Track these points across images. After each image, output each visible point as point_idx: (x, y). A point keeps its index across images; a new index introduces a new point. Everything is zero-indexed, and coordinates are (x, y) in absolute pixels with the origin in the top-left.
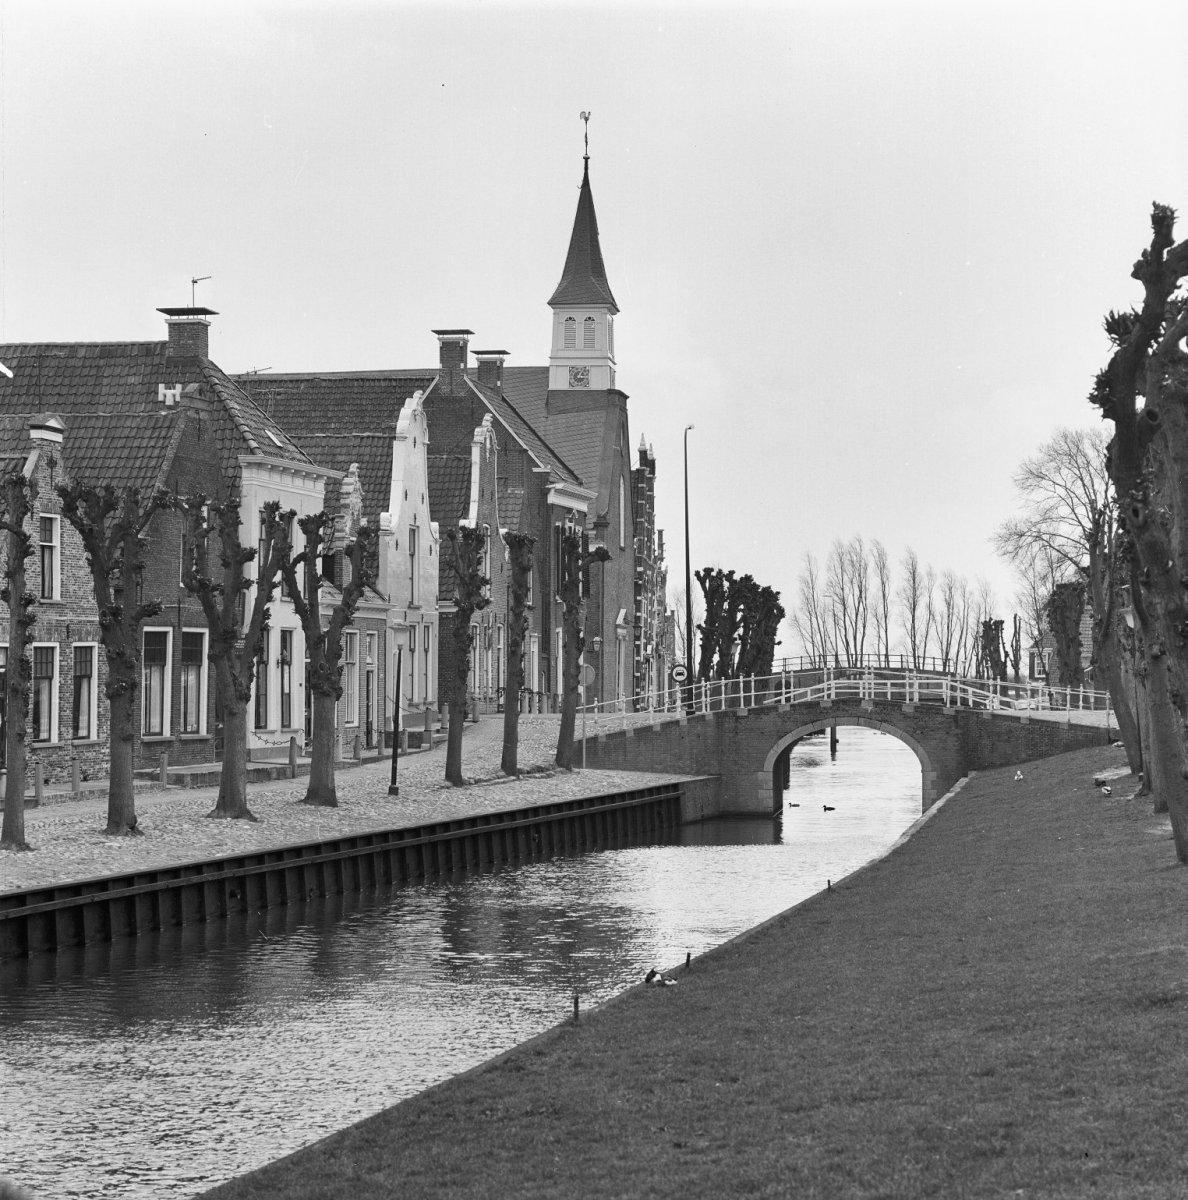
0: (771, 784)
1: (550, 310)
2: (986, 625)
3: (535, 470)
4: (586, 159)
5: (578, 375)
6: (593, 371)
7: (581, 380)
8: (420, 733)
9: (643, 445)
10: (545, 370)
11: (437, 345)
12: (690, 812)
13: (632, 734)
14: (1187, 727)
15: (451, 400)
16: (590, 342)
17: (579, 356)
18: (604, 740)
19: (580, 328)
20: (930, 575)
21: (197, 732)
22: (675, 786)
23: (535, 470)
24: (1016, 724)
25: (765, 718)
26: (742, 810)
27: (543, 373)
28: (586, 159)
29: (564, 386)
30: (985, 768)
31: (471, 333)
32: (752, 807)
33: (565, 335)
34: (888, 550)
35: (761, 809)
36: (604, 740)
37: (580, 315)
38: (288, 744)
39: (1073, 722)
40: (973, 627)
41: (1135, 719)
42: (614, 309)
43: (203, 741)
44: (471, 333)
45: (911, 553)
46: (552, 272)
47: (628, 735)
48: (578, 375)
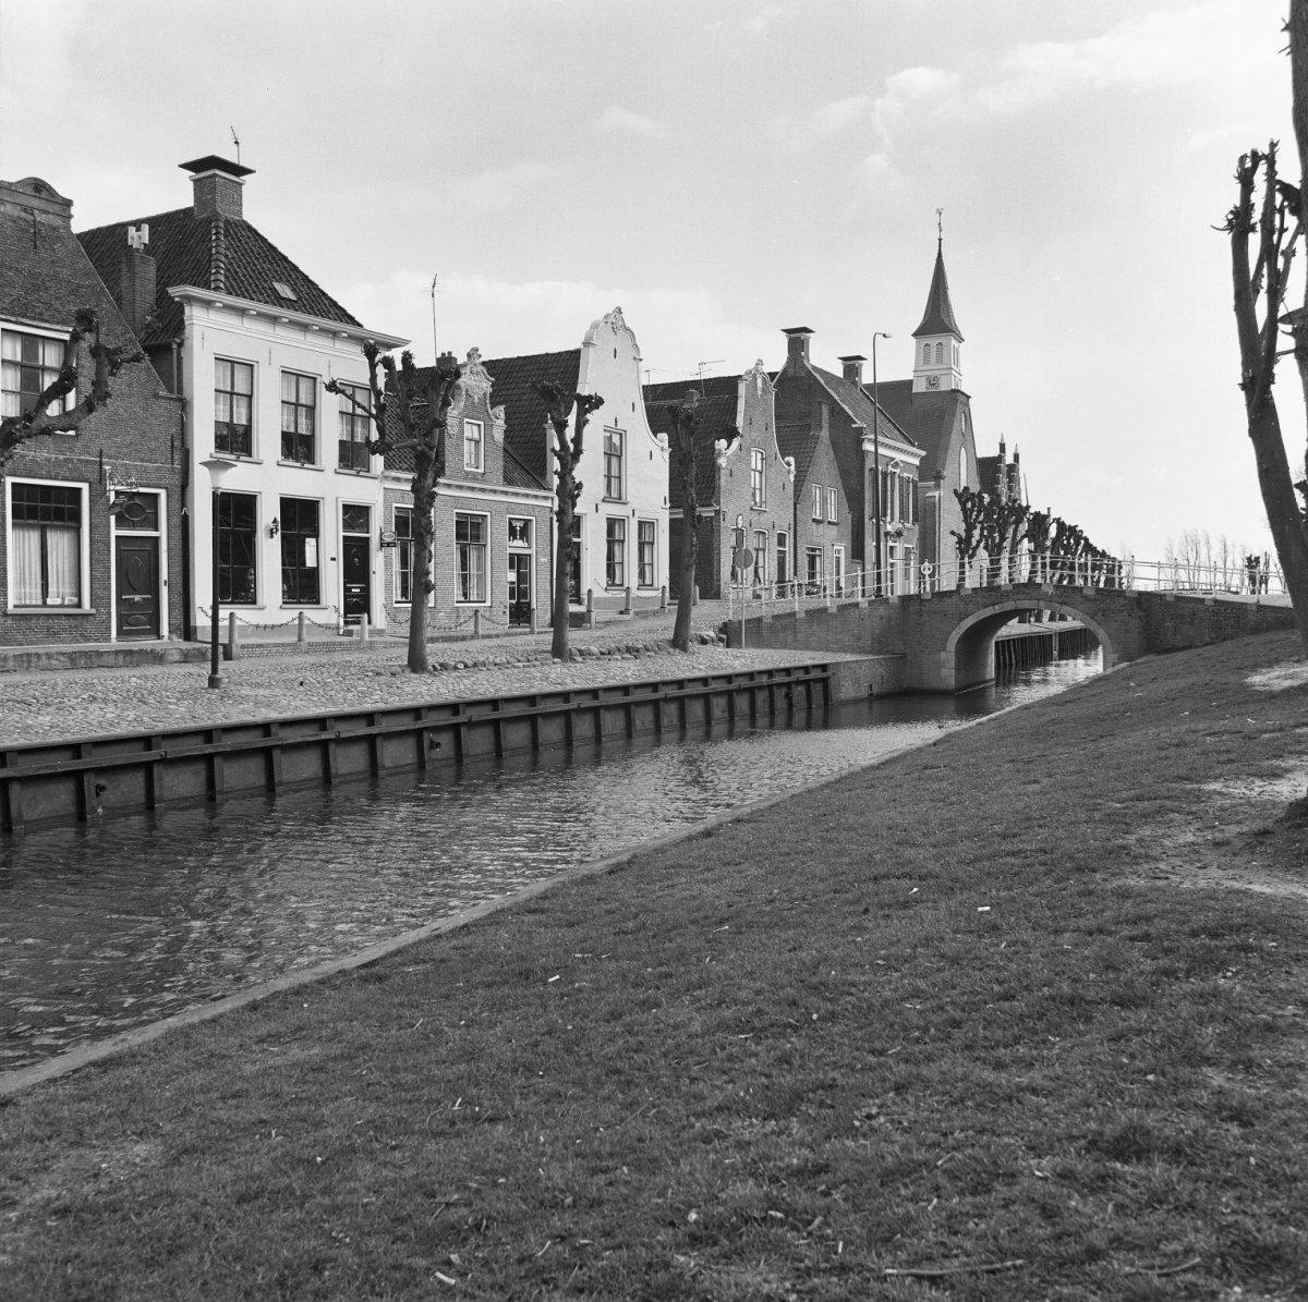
0: (953, 664)
1: (914, 340)
2: (1249, 559)
3: (854, 426)
4: (940, 240)
5: (932, 382)
6: (942, 378)
7: (934, 384)
8: (582, 614)
9: (1002, 439)
10: (911, 382)
11: (786, 341)
12: (846, 690)
13: (803, 615)
14: (110, 1289)
15: (795, 379)
16: (940, 359)
17: (933, 369)
18: (770, 620)
19: (933, 351)
20: (1233, 545)
21: (79, 605)
22: (824, 667)
23: (854, 426)
24: (1200, 606)
25: (948, 601)
26: (926, 687)
27: (909, 383)
28: (940, 240)
29: (924, 390)
30: (1167, 651)
31: (810, 331)
32: (935, 684)
33: (924, 356)
34: (1210, 535)
35: (943, 686)
36: (770, 620)
37: (933, 341)
38: (296, 622)
39: (1261, 603)
40: (1240, 563)
41: (1265, 271)
42: (961, 340)
43: (85, 616)
44: (810, 331)
45: (1223, 536)
46: (917, 316)
47: (798, 616)
48: (932, 382)
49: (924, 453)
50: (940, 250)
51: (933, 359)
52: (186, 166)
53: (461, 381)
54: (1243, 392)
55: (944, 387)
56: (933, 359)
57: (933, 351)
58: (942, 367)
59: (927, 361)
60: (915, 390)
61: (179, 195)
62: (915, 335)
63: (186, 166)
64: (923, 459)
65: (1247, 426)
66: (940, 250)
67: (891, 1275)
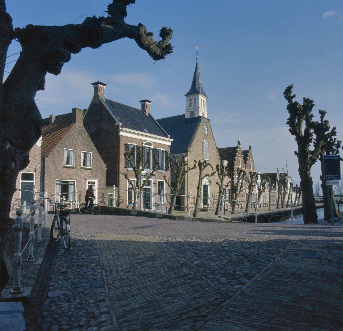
1: (185, 97)
19: (193, 102)
27: (184, 116)
48: (192, 113)
49: (172, 140)
50: (197, 64)
51: (193, 105)
52: (92, 84)
53: (49, 211)
54: (80, 21)
55: (196, 116)
56: (193, 105)
57: (193, 102)
58: (191, 108)
59: (190, 105)
60: (310, 143)
61: (71, 111)
62: (186, 95)
63: (92, 84)
64: (172, 143)
65: (35, 24)
66: (197, 64)
67: (224, 278)
